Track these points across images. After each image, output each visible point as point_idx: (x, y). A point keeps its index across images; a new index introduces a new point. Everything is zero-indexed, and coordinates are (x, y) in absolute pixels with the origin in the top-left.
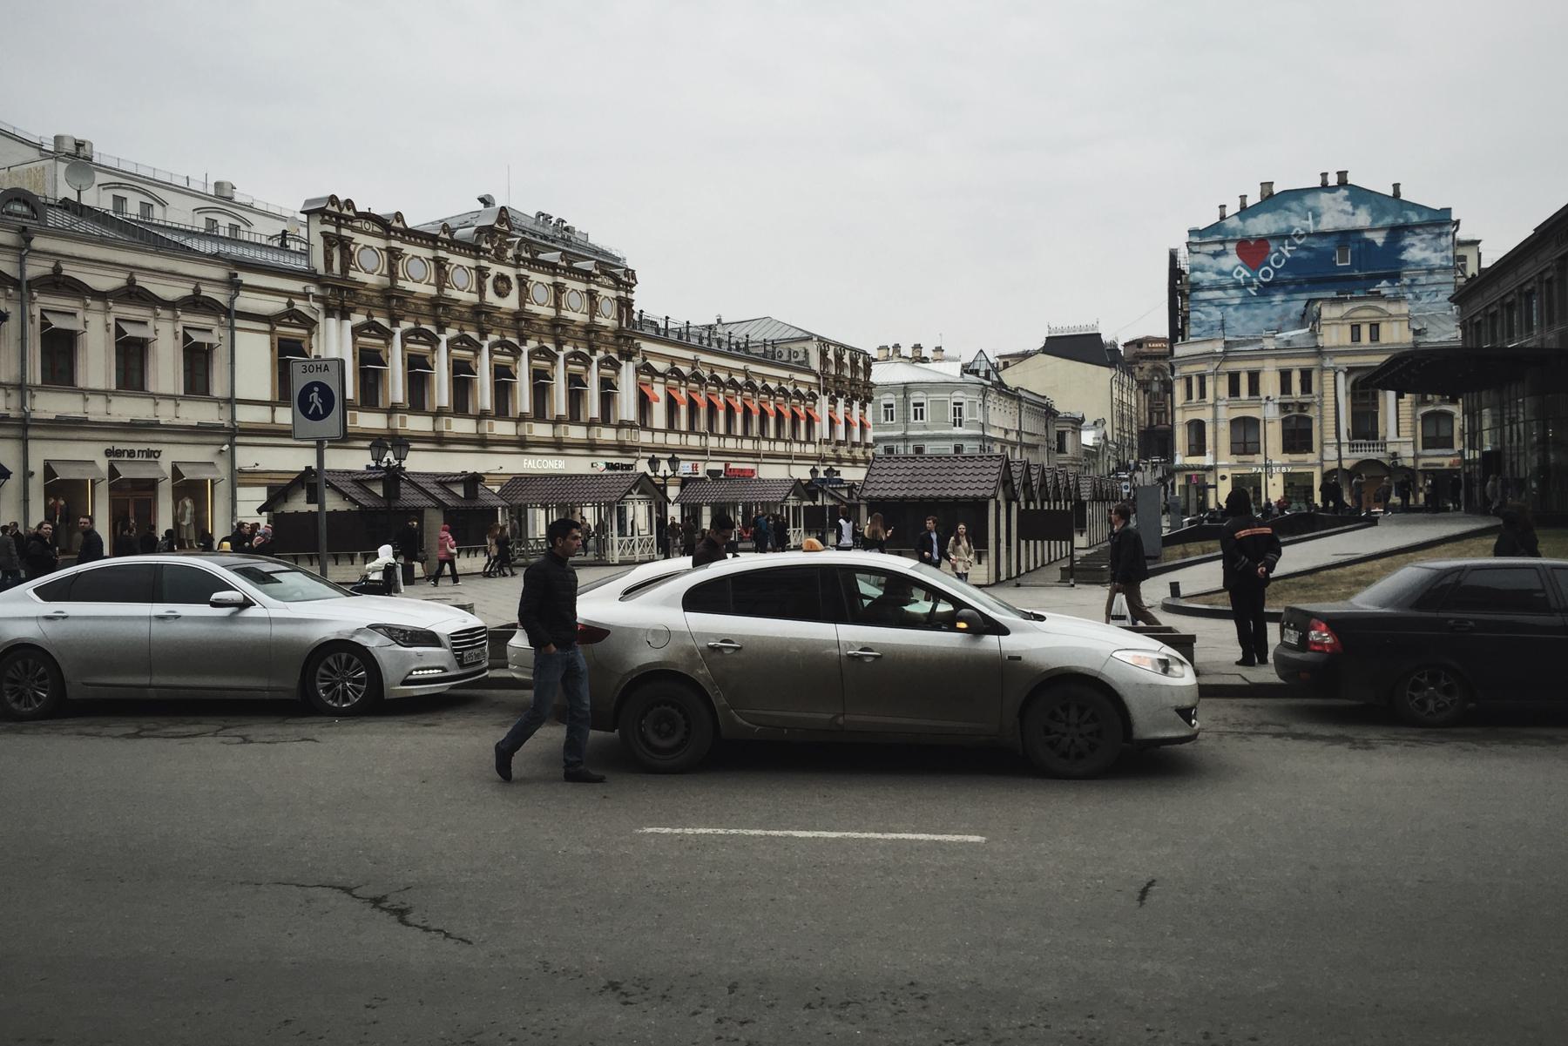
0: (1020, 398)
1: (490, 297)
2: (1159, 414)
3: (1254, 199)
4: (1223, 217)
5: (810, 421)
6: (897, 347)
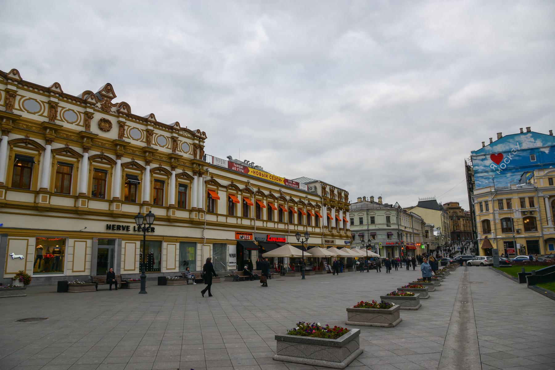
0: (412, 216)
1: (94, 129)
2: (456, 226)
3: (495, 139)
4: (484, 146)
5: (317, 217)
6: (364, 198)
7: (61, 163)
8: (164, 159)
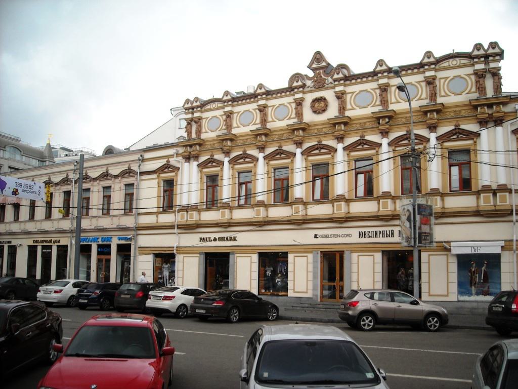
1: (309, 116)
7: (452, 152)
8: (463, 113)
